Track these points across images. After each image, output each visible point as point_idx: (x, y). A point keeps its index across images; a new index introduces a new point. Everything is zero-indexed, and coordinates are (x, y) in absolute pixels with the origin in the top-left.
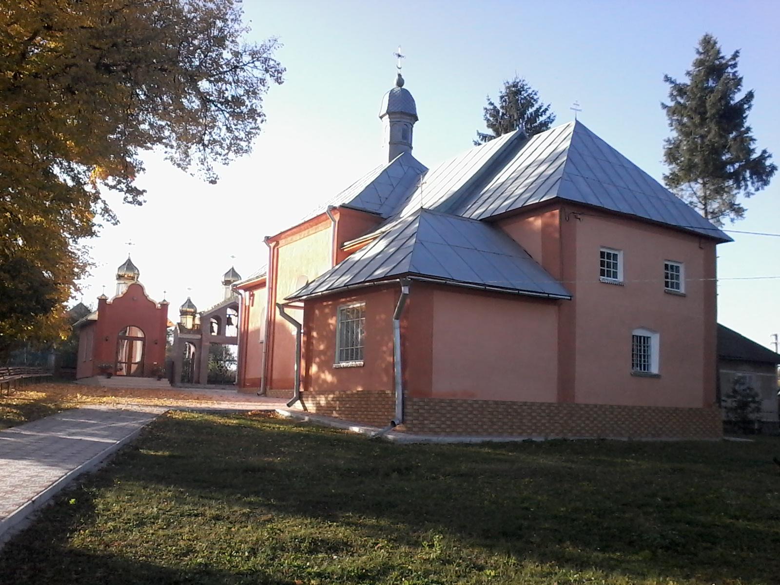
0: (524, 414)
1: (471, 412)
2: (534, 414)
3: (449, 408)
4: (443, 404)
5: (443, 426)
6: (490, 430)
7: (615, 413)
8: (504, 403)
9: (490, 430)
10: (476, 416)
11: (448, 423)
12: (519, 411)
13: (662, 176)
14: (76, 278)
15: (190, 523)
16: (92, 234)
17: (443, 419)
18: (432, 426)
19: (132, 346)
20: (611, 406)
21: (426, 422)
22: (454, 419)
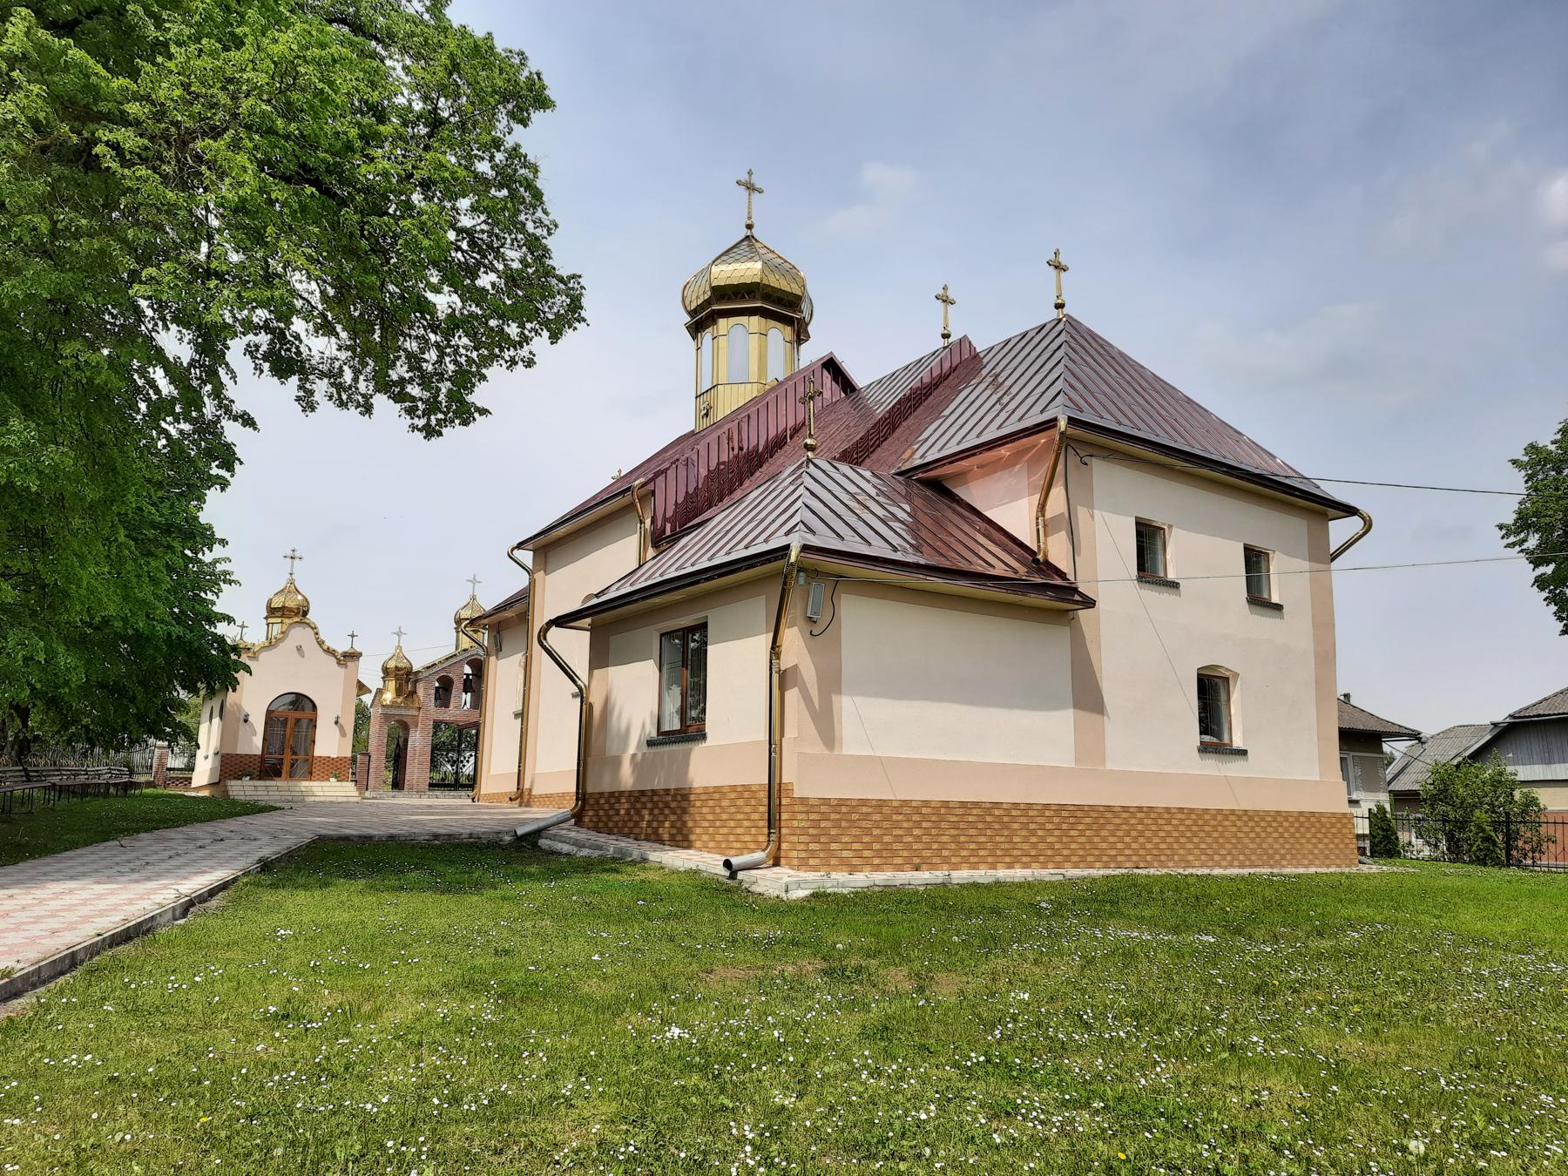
0: (1016, 826)
1: (918, 825)
2: (1032, 826)
3: (877, 817)
4: (865, 809)
5: (866, 853)
6: (954, 860)
7: (1174, 822)
8: (977, 805)
9: (954, 860)
10: (927, 832)
11: (876, 846)
12: (1006, 819)
13: (319, 409)
14: (169, 419)
15: (1480, 959)
16: (525, 126)
17: (866, 839)
18: (845, 854)
19: (1260, 476)
20: (1168, 810)
21: (834, 846)
22: (887, 839)
